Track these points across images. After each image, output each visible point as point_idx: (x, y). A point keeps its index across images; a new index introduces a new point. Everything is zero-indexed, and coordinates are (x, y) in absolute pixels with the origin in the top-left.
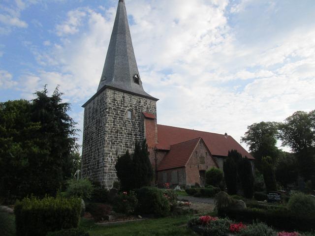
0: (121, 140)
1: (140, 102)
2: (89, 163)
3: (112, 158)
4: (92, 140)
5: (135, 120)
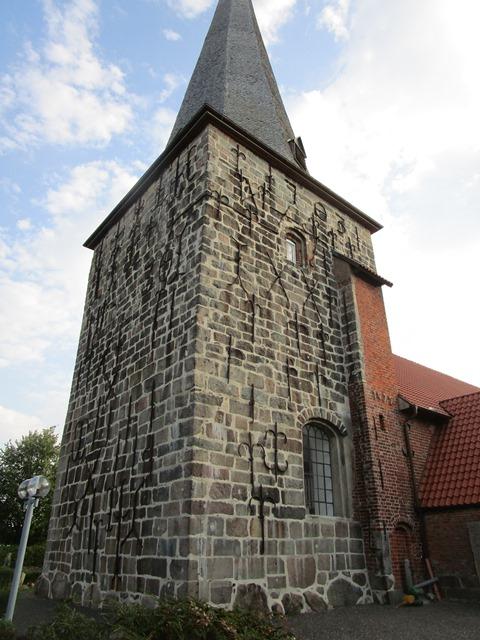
0: (269, 344)
1: (324, 217)
2: (97, 455)
3: (232, 427)
4: (118, 349)
5: (315, 276)
